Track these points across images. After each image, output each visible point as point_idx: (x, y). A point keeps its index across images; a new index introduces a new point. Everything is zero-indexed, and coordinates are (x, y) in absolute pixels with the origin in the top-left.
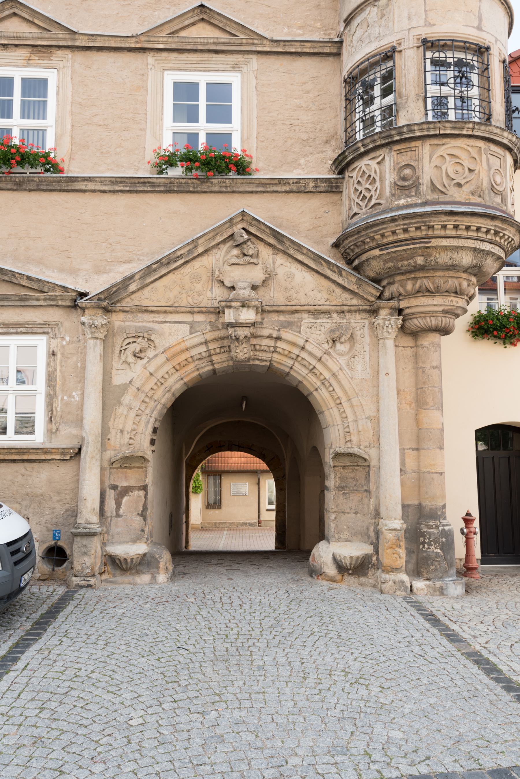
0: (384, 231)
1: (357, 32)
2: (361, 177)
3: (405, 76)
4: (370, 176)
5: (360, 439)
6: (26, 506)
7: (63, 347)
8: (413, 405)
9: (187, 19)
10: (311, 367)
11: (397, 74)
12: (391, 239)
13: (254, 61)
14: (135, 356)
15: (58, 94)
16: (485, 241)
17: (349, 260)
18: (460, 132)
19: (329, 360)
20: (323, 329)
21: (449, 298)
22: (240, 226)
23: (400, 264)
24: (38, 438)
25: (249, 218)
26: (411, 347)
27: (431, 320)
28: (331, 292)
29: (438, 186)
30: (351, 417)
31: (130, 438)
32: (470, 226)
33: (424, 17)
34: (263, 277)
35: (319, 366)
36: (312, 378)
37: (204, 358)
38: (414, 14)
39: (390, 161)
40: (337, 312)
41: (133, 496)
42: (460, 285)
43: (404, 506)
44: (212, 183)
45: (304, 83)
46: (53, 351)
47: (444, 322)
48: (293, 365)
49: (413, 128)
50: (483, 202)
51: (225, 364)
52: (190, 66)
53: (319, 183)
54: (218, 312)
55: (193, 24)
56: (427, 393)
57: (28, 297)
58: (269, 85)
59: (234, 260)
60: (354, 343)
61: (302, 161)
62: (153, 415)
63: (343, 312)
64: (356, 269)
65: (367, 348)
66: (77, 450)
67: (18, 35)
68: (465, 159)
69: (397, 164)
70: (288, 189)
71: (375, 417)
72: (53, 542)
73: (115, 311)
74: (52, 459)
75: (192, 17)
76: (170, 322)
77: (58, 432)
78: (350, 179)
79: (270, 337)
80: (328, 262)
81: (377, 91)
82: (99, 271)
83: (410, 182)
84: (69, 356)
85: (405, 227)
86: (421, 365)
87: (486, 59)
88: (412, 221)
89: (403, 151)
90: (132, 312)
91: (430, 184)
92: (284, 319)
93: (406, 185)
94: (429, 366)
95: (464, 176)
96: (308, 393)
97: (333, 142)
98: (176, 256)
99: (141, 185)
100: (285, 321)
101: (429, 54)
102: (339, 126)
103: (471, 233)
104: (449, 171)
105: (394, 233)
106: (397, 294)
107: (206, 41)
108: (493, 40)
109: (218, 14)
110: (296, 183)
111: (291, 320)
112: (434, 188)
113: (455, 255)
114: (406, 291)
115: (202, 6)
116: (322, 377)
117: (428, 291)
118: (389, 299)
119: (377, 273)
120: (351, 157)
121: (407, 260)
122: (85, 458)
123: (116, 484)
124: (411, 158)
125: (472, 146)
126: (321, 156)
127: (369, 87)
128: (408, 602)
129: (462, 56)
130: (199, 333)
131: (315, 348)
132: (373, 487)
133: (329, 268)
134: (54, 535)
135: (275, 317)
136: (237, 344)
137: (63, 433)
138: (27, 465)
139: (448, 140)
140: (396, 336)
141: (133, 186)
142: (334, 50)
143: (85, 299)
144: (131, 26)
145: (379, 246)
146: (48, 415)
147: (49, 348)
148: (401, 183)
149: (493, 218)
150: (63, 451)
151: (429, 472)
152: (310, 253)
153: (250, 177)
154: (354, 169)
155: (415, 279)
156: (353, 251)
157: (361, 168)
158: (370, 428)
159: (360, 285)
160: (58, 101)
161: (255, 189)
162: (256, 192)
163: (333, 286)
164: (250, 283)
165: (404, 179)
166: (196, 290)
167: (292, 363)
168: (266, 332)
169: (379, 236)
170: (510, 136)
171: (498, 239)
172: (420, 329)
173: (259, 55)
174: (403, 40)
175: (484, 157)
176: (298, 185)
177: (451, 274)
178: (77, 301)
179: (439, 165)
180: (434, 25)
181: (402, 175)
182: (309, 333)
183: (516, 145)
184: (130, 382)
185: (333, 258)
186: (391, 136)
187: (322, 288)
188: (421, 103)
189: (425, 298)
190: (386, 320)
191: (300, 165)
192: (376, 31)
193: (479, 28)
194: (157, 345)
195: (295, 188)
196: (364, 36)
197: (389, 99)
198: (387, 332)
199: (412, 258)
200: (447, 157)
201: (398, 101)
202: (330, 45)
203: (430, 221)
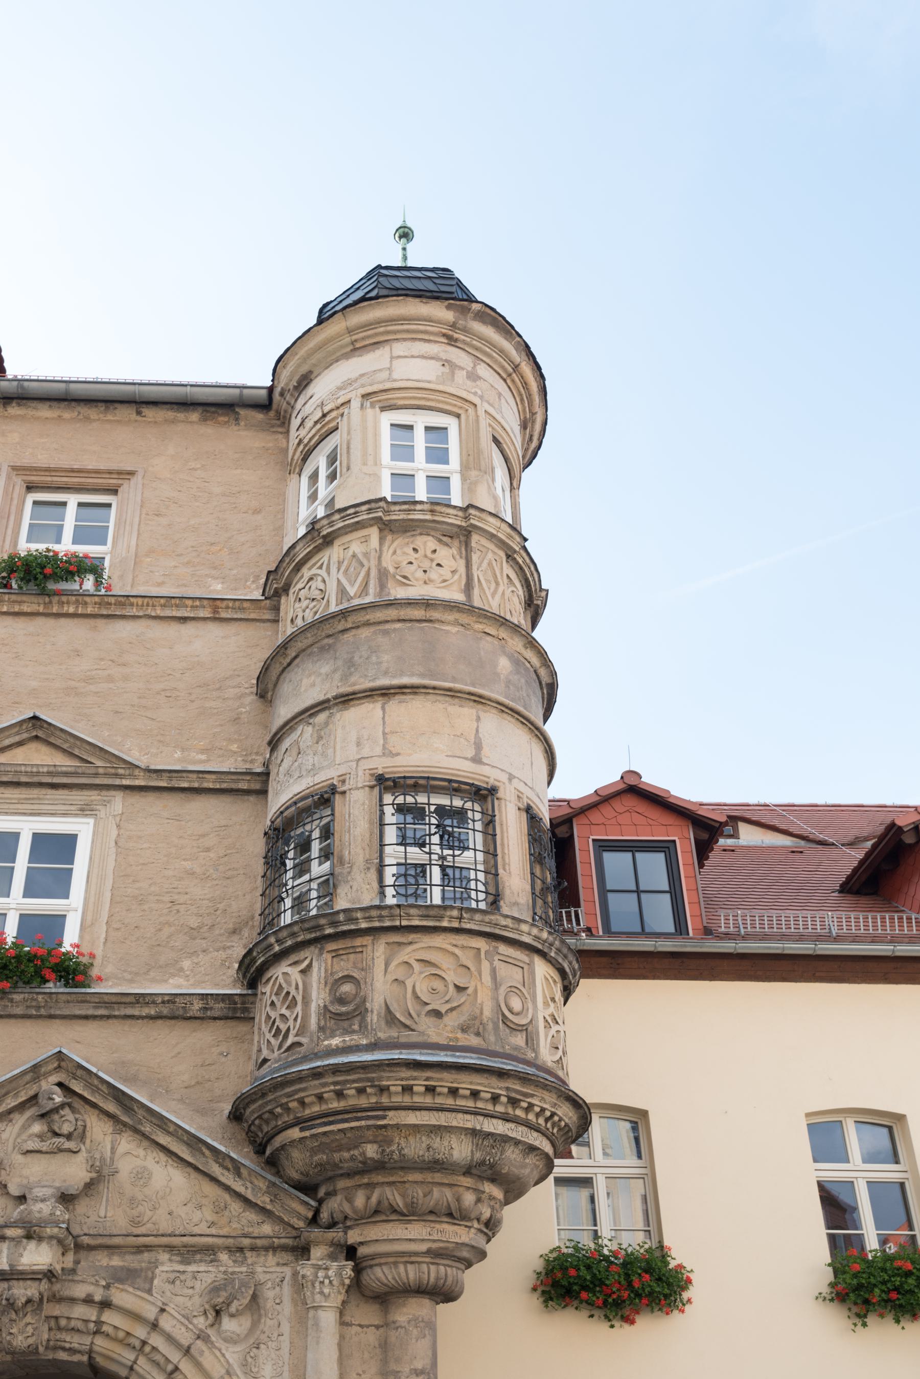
0: (302, 1094)
2: (277, 994)
3: (349, 831)
9: (8, 737)
10: (170, 1367)
11: (337, 827)
12: (316, 1109)
13: (118, 802)
16: (492, 1117)
17: (260, 1144)
18: (437, 924)
19: (207, 1353)
20: (198, 1285)
21: (437, 1226)
22: (54, 1079)
23: (337, 1156)
25: (70, 1065)
26: (377, 1327)
27: (406, 1271)
28: (220, 1209)
29: (398, 1016)
33: (382, 742)
38: (366, 737)
39: (320, 969)
40: (228, 1249)
42: (458, 1200)
44: (11, 1000)
47: (433, 1275)
48: (135, 1362)
49: (354, 915)
50: (484, 1045)
52: (6, 806)
53: (211, 1003)
55: (20, 744)
58: (140, 837)
60: (260, 1316)
61: (186, 964)
63: (241, 1250)
65: (286, 1328)
68: (449, 969)
69: (332, 974)
70: (153, 1012)
75: (18, 734)
79: (88, 1300)
83: (351, 1007)
85: (338, 1087)
86: (393, 1366)
88: (349, 1078)
89: (341, 952)
92: (121, 1264)
93: (346, 1011)
94: (407, 1370)
95: (447, 998)
97: (246, 933)
100: (122, 1268)
101: (388, 798)
107: (35, 770)
108: (504, 778)
109: (62, 730)
110: (168, 1001)
112: (390, 1018)
113: (436, 1143)
114: (355, 1211)
115: (35, 718)
117: (395, 1211)
118: (332, 1225)
119: (302, 1173)
120: (262, 959)
121: (349, 1150)
124: (355, 966)
125: (463, 947)
126: (222, 955)
127: (304, 847)
129: (444, 801)
131: (178, 1326)
133: (217, 1162)
135: (103, 1259)
136: (14, 1316)
139: (419, 936)
140: (344, 1302)
142: (257, 785)
145: (299, 1122)
149: (501, 1074)
152: (180, 1132)
153: (83, 990)
155: (371, 1186)
156: (260, 1128)
157: (277, 978)
159: (275, 1196)
161: (91, 1012)
162: (94, 1017)
163: (227, 1197)
164: (58, 1188)
165: (341, 1001)
167: (132, 1357)
168: (80, 1291)
172: (388, 1290)
173: (127, 792)
174: (348, 776)
175: (485, 966)
176: (171, 1006)
177: (438, 1177)
179: (401, 978)
180: (398, 754)
182: (168, 1294)
183: (551, 945)
185: (222, 1140)
186: (319, 927)
187: (204, 1201)
188: (373, 875)
189: (391, 1224)
190: (319, 1268)
191: (181, 969)
192: (309, 760)
193: (477, 759)
195: (165, 1011)
196: (293, 768)
198: (321, 1293)
199: (356, 1147)
200: (416, 966)
201: (338, 870)
202: (248, 778)
203: (380, 1079)
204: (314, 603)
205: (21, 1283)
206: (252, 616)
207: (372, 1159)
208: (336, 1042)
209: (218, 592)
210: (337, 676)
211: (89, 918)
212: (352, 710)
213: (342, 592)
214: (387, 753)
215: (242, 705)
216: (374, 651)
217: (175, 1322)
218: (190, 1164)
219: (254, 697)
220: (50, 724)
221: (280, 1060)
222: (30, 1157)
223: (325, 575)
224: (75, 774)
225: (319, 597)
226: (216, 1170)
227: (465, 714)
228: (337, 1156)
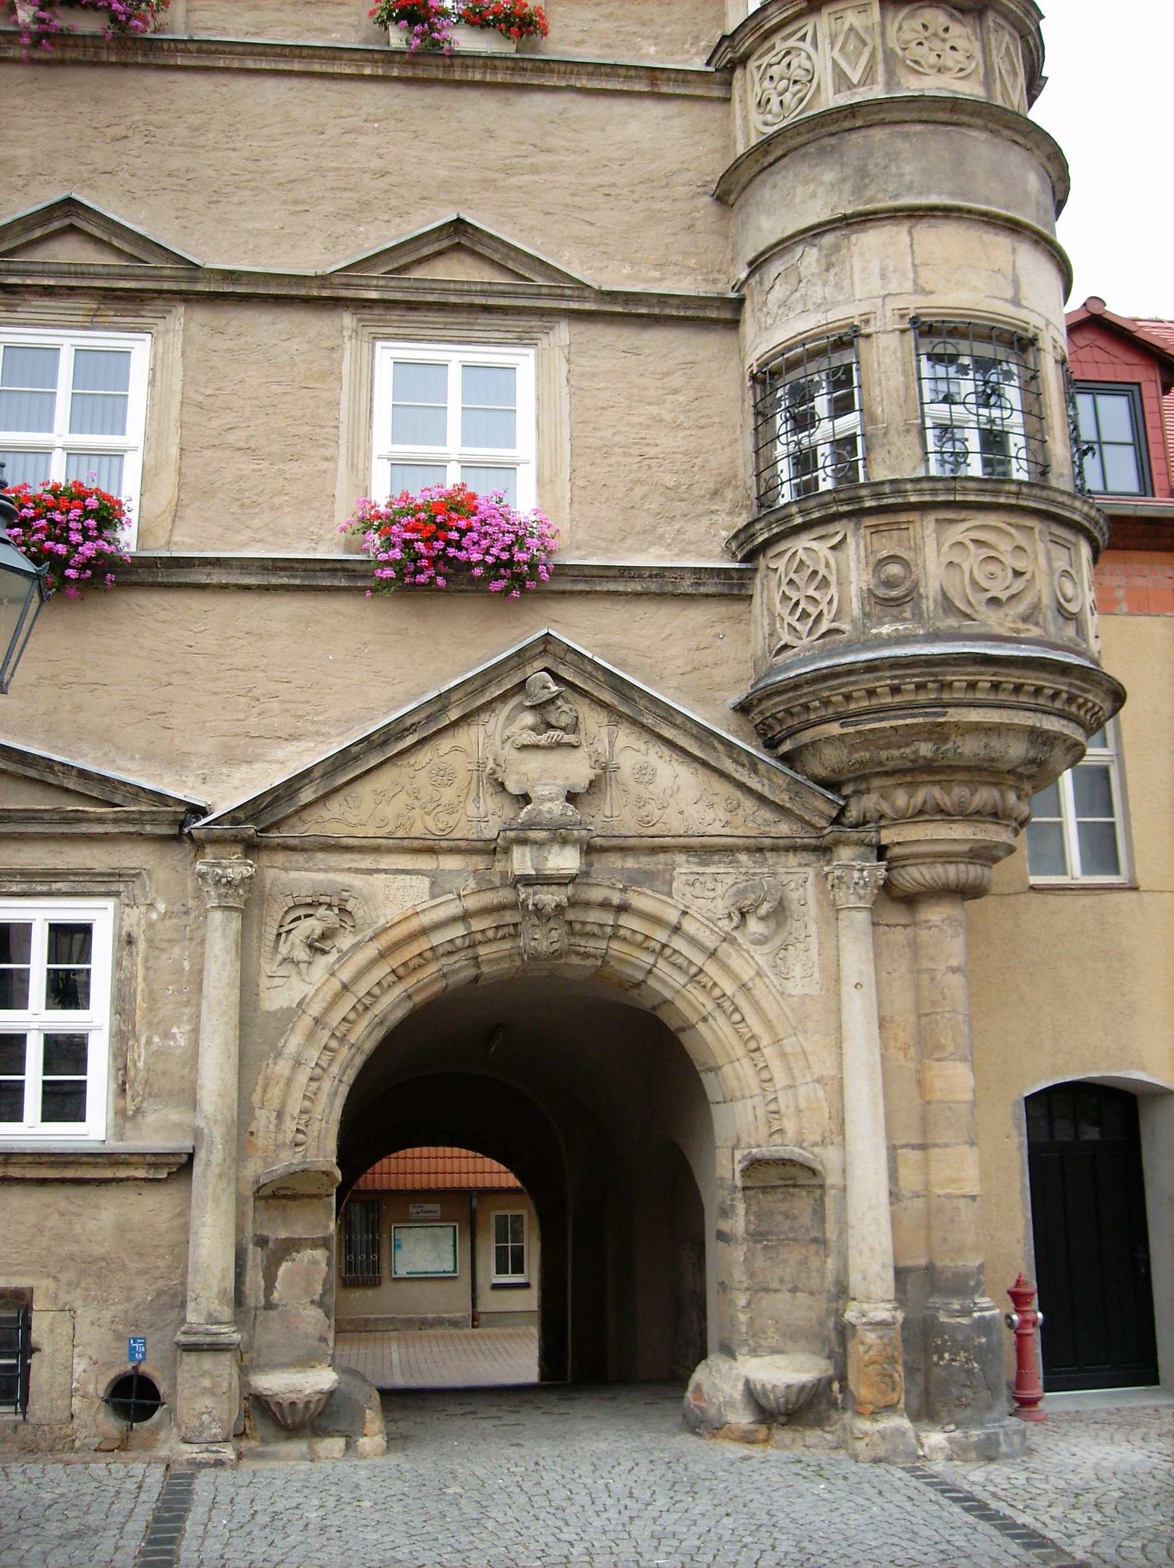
1: (777, 287)
4: (815, 573)
5: (802, 1128)
6: (69, 1284)
7: (151, 925)
8: (912, 1051)
10: (693, 970)
13: (563, 332)
14: (310, 946)
15: (152, 383)
16: (1050, 713)
17: (772, 738)
19: (734, 955)
22: (539, 664)
23: (884, 754)
24: (93, 1129)
30: (781, 1079)
31: (298, 1130)
32: (1022, 685)
33: (911, 275)
34: (591, 774)
35: (711, 968)
36: (696, 995)
37: (459, 950)
39: (858, 547)
41: (302, 1260)
43: (901, 1274)
45: (668, 374)
46: (129, 935)
51: (505, 965)
53: (704, 577)
54: (492, 850)
55: (439, 254)
56: (941, 1026)
57: (80, 815)
58: (594, 375)
59: (530, 738)
61: (668, 530)
62: (345, 1078)
63: (760, 850)
64: (788, 759)
65: (813, 929)
66: (185, 1158)
67: (79, 269)
71: (833, 1078)
72: (130, 1366)
73: (266, 847)
74: (128, 1179)
76: (386, 871)
77: (139, 1117)
78: (771, 574)
79: (605, 905)
80: (729, 745)
81: (821, 404)
82: (231, 758)
84: (165, 945)
87: (1031, 359)
90: (304, 850)
91: (940, 597)
92: (636, 866)
93: (893, 596)
94: (943, 968)
96: (681, 1024)
97: (729, 494)
98: (402, 727)
99: (326, 574)
100: (638, 870)
102: (740, 461)
103: (1023, 698)
104: (976, 573)
105: (871, 693)
106: (876, 815)
108: (1041, 323)
110: (656, 576)
111: (651, 867)
112: (947, 605)
116: (717, 992)
117: (940, 810)
118: (855, 826)
122: (204, 1176)
123: (265, 1233)
127: (802, 394)
128: (918, 1477)
130: (451, 896)
131: (702, 928)
132: (831, 1233)
133: (730, 757)
134: (132, 1349)
135: (616, 861)
137: (150, 1118)
138: (71, 1191)
141: (309, 577)
143: (204, 821)
144: (313, 257)
146: (116, 1078)
147: (121, 928)
148: (882, 592)
150: (154, 1160)
151: (949, 1196)
152: (689, 724)
154: (779, 555)
158: (824, 1103)
159: (797, 794)
160: (151, 397)
163: (738, 794)
165: (889, 584)
166: (444, 801)
167: (651, 960)
168: (597, 894)
169: (840, 698)
170: (1086, 509)
171: (1074, 709)
178: (181, 826)
180: (932, 292)
181: (883, 576)
184: (300, 1004)
186: (859, 499)
187: (715, 799)
188: (914, 438)
193: (1016, 302)
194: (359, 922)
195: (653, 587)
196: (793, 298)
197: (849, 423)
199: (907, 745)
204: (798, 87)
205: (545, 888)
206: (698, 92)
207: (925, 758)
208: (886, 629)
209: (652, 58)
210: (847, 187)
211: (547, 473)
212: (871, 232)
213: (841, 78)
214: (919, 290)
215: (696, 209)
216: (893, 157)
217: (698, 925)
218: (696, 759)
219: (707, 199)
220: (476, 229)
221: (812, 648)
222: (525, 755)
223: (811, 51)
224: (515, 294)
225: (804, 80)
226: (729, 766)
227: (1001, 243)
228: (884, 754)
